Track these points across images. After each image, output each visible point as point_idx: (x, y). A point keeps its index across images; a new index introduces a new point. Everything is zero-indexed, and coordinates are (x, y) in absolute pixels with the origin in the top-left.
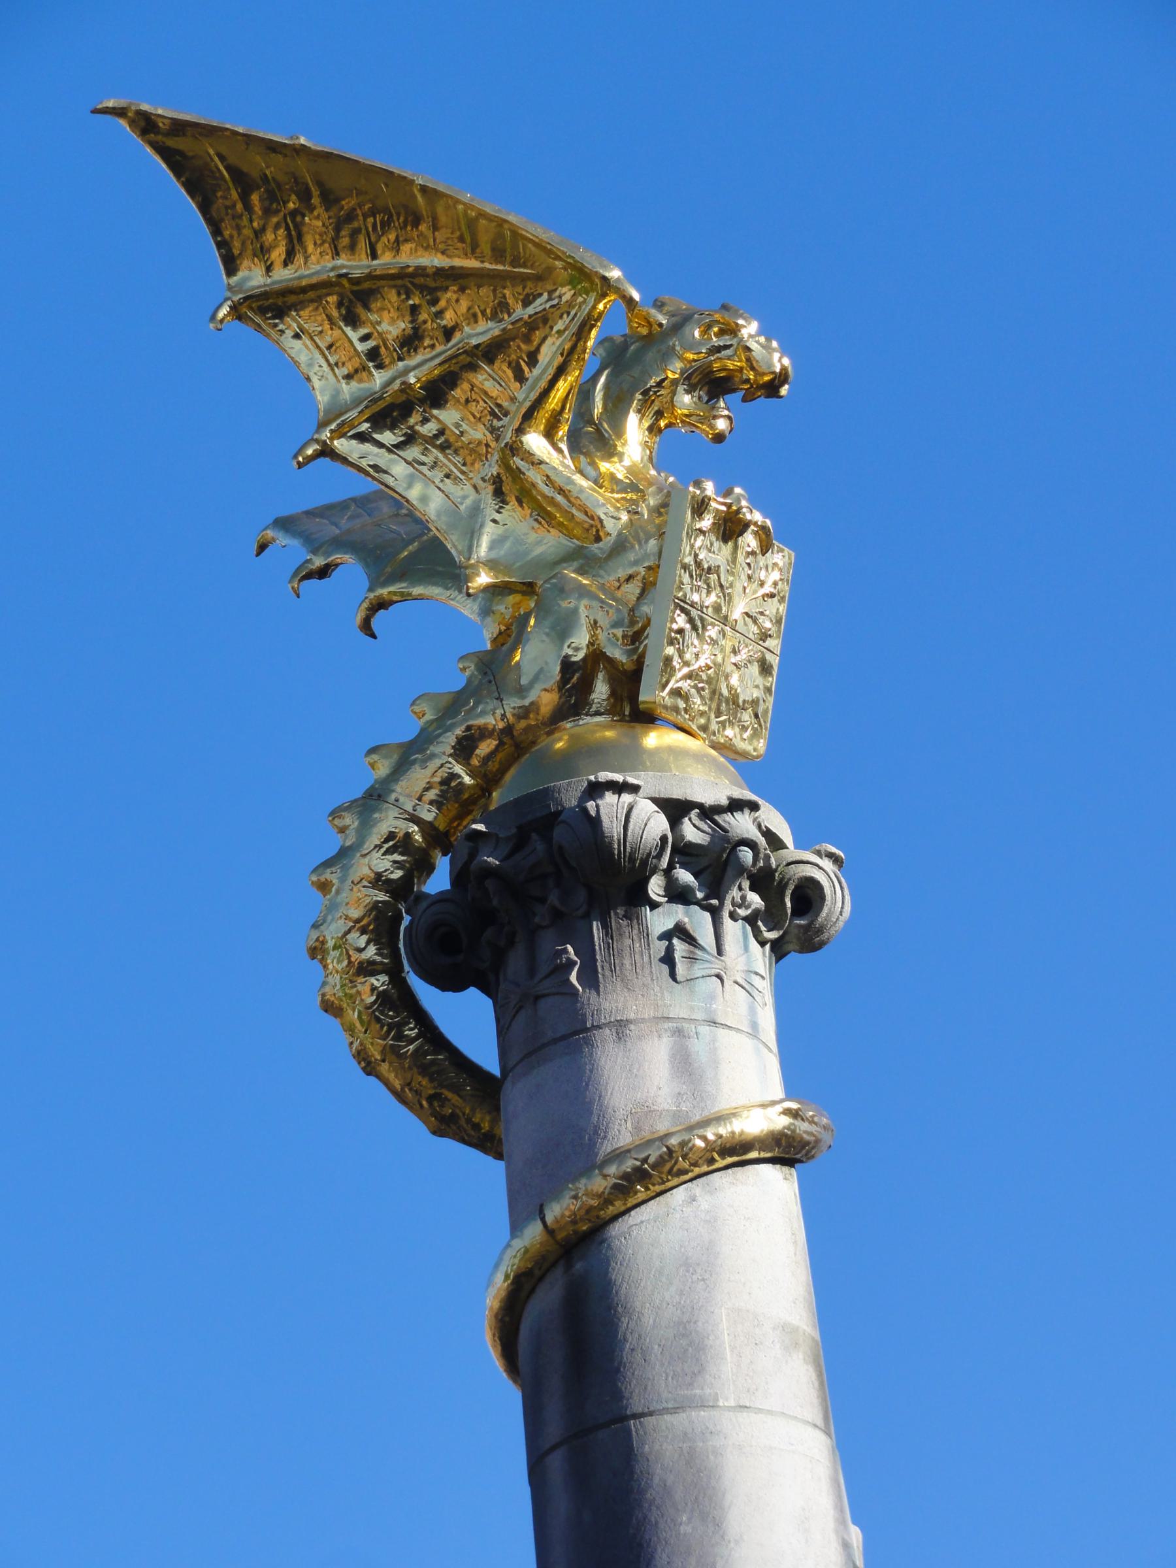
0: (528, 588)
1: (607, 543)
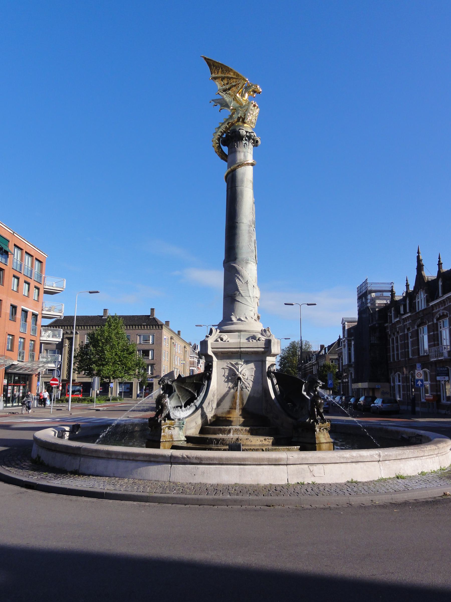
0: (235, 109)
1: (243, 106)
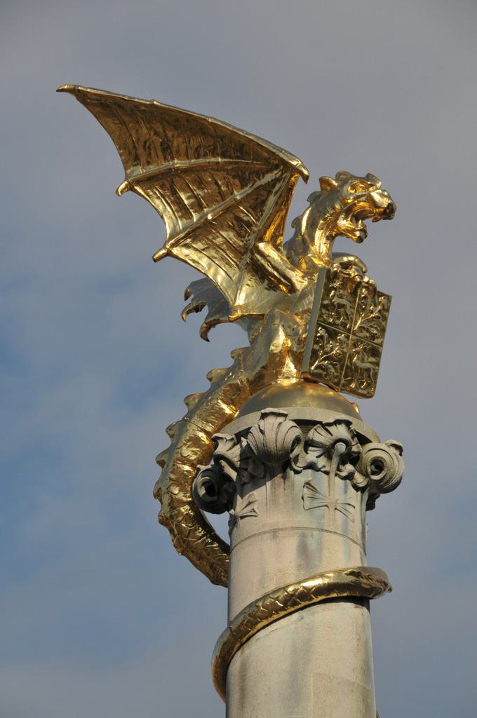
1: (298, 293)
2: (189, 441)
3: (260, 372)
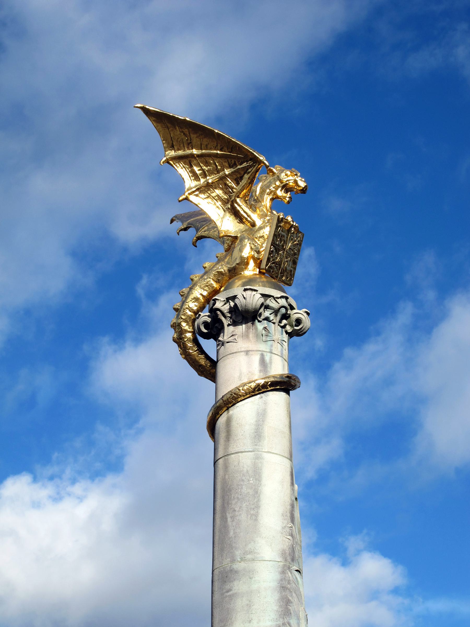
2: (193, 299)
3: (235, 266)
